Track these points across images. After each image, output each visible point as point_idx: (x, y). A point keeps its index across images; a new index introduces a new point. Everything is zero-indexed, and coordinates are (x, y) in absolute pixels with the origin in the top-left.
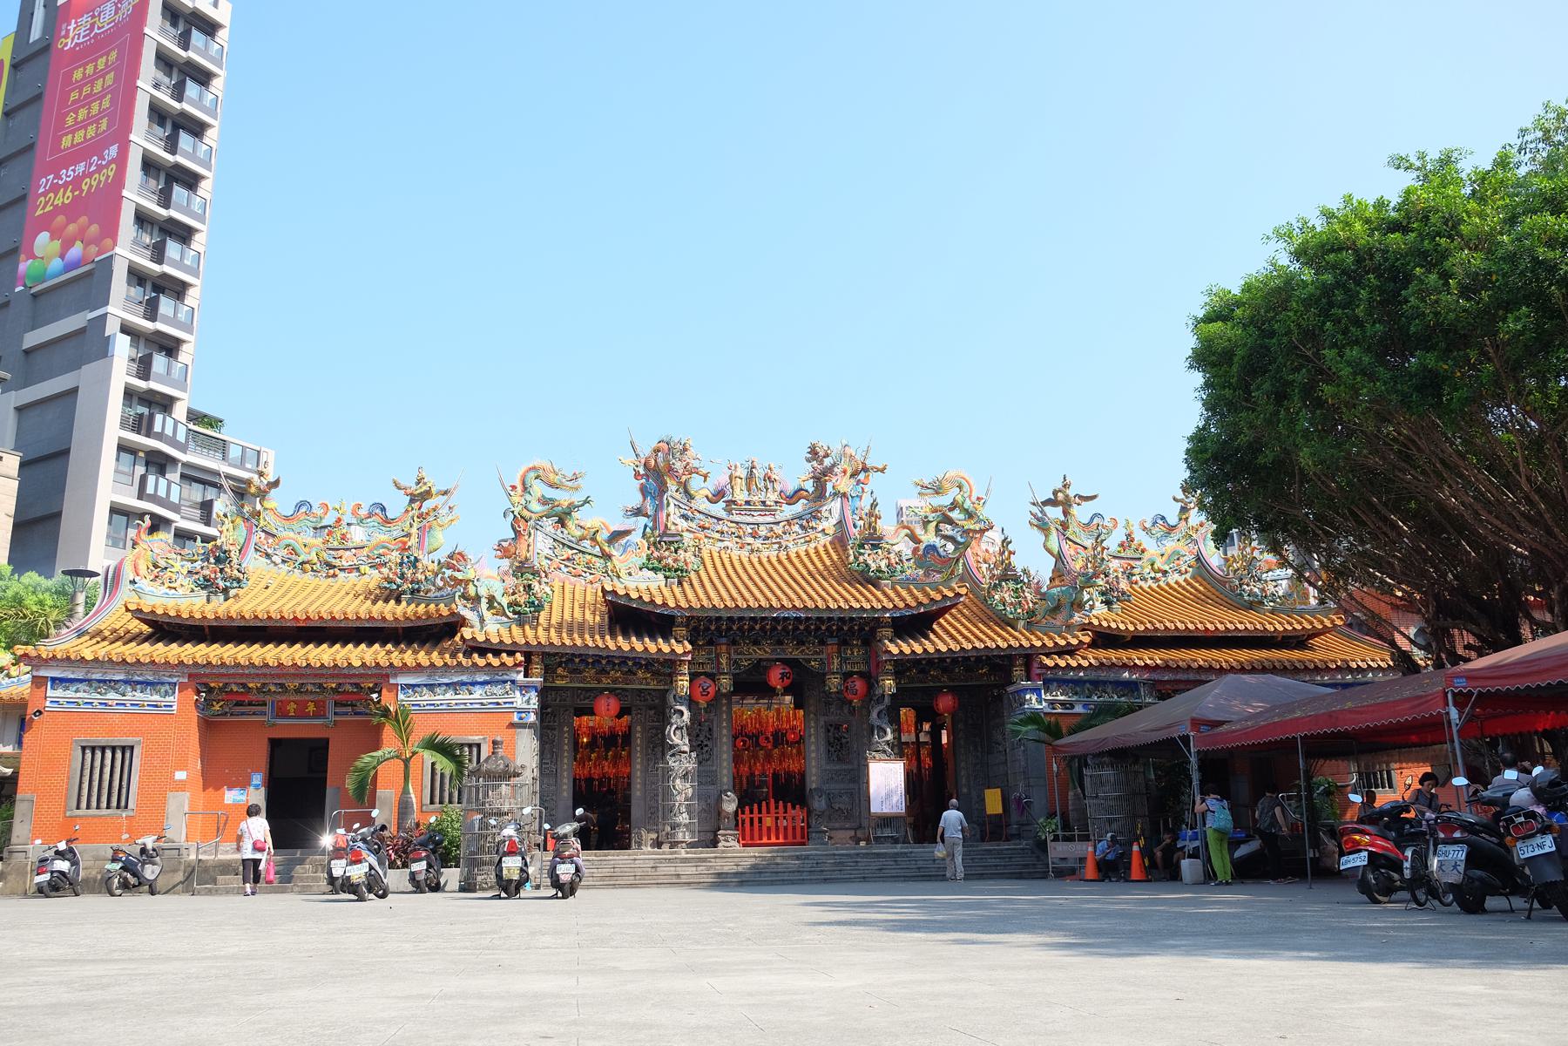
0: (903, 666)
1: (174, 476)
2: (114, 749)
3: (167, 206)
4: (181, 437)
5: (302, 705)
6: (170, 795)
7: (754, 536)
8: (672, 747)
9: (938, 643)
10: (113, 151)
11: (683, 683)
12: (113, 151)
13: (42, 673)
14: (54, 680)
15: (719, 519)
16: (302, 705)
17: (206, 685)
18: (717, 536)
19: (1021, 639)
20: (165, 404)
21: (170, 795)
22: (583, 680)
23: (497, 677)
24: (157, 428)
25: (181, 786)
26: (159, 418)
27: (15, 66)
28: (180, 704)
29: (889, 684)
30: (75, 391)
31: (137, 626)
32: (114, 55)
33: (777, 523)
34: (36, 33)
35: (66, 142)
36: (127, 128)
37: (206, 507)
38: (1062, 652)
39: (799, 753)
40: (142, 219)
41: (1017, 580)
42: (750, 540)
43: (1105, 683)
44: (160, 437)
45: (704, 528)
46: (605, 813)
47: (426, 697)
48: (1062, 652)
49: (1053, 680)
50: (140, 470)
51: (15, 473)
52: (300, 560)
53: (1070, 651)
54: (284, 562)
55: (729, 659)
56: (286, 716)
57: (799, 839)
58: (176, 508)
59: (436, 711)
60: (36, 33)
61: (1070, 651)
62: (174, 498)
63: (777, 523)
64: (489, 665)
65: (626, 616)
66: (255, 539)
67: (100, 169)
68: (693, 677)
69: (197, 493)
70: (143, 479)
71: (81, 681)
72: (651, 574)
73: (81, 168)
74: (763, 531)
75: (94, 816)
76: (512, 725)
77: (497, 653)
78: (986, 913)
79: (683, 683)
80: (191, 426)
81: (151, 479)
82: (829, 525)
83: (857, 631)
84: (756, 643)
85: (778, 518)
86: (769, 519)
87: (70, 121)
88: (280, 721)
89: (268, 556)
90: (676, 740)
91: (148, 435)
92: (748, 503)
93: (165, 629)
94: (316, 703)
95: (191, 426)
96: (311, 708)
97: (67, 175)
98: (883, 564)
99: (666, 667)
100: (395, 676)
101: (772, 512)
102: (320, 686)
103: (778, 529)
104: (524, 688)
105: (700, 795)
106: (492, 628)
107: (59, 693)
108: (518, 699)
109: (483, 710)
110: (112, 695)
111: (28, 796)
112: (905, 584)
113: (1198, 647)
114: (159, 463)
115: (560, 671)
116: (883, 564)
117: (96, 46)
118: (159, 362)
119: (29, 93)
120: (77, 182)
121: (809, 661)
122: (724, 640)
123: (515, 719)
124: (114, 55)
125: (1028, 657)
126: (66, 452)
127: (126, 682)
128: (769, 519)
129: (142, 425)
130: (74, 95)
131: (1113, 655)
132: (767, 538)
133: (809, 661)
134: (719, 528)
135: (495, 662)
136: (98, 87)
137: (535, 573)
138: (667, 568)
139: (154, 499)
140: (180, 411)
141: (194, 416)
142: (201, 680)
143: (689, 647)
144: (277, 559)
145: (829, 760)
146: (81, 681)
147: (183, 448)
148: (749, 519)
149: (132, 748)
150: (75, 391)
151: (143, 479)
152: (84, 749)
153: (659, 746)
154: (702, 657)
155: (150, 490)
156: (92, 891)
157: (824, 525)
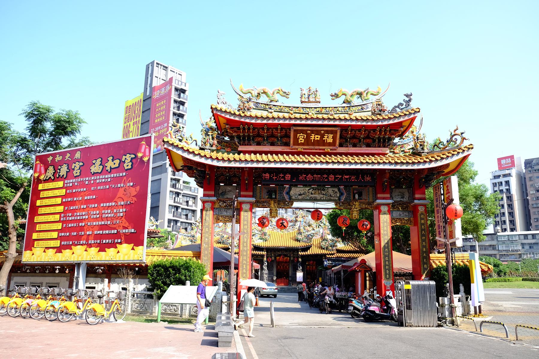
0: (302, 256)
1: (180, 196)
3: (180, 98)
9: (309, 252)
10: (166, 125)
11: (265, 259)
12: (166, 125)
19: (324, 252)
20: (178, 180)
27: (144, 101)
29: (300, 260)
32: (165, 101)
34: (148, 94)
35: (156, 121)
36: (169, 120)
37: (187, 202)
38: (330, 254)
39: (82, 323)
40: (174, 114)
44: (178, 189)
48: (330, 254)
49: (329, 259)
50: (174, 196)
53: (333, 254)
58: (181, 204)
60: (148, 94)
61: (333, 254)
62: (181, 202)
67: (163, 128)
68: (267, 258)
69: (185, 199)
70: (175, 198)
73: (159, 127)
78: (492, 302)
81: (176, 198)
82: (297, 227)
83: (294, 250)
87: (157, 116)
97: (157, 129)
99: (263, 256)
112: (304, 242)
113: (529, 211)
114: (178, 194)
117: (161, 98)
118: (181, 107)
119: (147, 102)
120: (159, 131)
124: (165, 101)
125: (325, 255)
129: (174, 186)
130: (157, 110)
131: (340, 255)
136: (162, 109)
139: (177, 203)
140: (181, 182)
147: (182, 190)
151: (175, 198)
155: (176, 201)
156: (158, 201)
157: (296, 227)
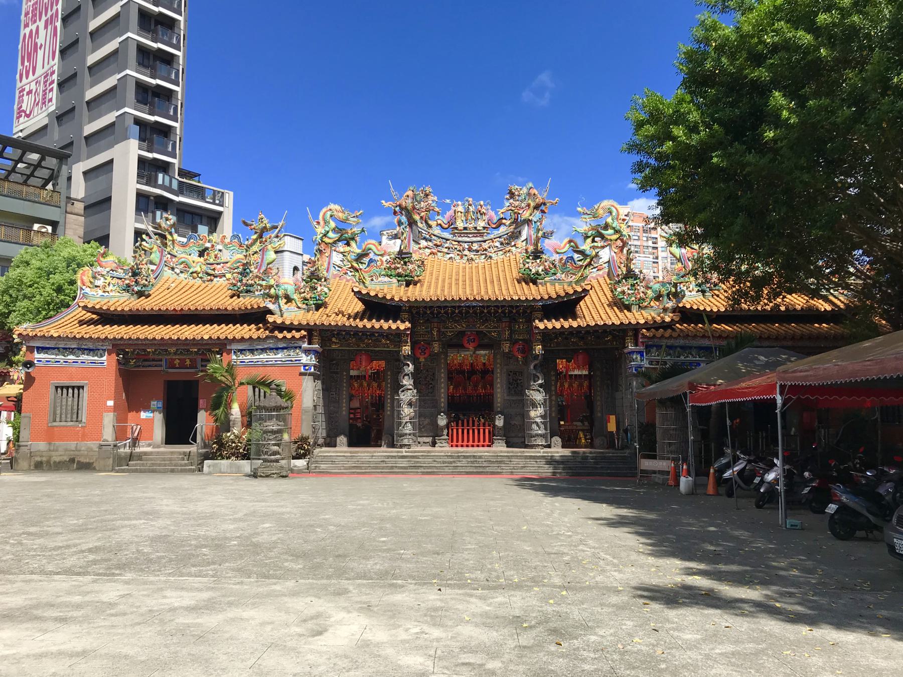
2: (73, 388)
4: (175, 185)
5: (183, 361)
6: (105, 414)
7: (470, 250)
8: (403, 386)
13: (32, 344)
14: (38, 348)
15: (447, 240)
16: (183, 361)
17: (123, 350)
18: (445, 250)
21: (105, 414)
22: (349, 345)
23: (291, 345)
24: (160, 182)
25: (108, 409)
26: (160, 176)
28: (107, 361)
29: (538, 349)
30: (111, 161)
31: (89, 316)
33: (485, 241)
41: (635, 277)
42: (466, 252)
43: (691, 348)
45: (437, 246)
46: (363, 424)
47: (249, 357)
51: (82, 212)
52: (191, 271)
54: (181, 272)
55: (439, 331)
56: (174, 367)
57: (487, 443)
59: (254, 365)
63: (485, 241)
64: (285, 337)
65: (375, 307)
66: (165, 259)
71: (54, 348)
72: (387, 279)
74: (475, 246)
75: (64, 426)
76: (301, 374)
77: (289, 330)
79: (406, 349)
80: (181, 179)
84: (456, 321)
85: (485, 238)
86: (479, 239)
88: (170, 370)
89: (173, 269)
90: (405, 382)
91: (155, 187)
92: (465, 228)
93: (107, 317)
94: (191, 360)
95: (181, 179)
96: (188, 362)
98: (540, 269)
100: (230, 344)
101: (481, 235)
102: (188, 350)
103: (485, 245)
104: (307, 352)
105: (420, 415)
106: (292, 314)
107: (42, 356)
108: (305, 359)
109: (283, 365)
110: (71, 357)
111: (28, 414)
115: (334, 339)
116: (540, 269)
121: (490, 332)
122: (436, 320)
123: (302, 370)
126: (109, 199)
127: (78, 349)
128: (479, 239)
132: (477, 251)
133: (490, 332)
134: (446, 245)
135: (289, 336)
137: (319, 279)
138: (399, 275)
141: (182, 173)
142: (117, 346)
143: (409, 325)
144: (178, 271)
145: (509, 394)
146: (54, 348)
148: (468, 239)
149: (83, 387)
150: (111, 161)
152: (57, 388)
153: (397, 387)
154: (421, 329)
